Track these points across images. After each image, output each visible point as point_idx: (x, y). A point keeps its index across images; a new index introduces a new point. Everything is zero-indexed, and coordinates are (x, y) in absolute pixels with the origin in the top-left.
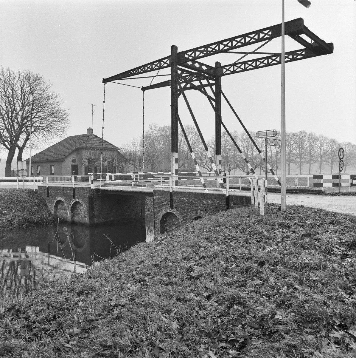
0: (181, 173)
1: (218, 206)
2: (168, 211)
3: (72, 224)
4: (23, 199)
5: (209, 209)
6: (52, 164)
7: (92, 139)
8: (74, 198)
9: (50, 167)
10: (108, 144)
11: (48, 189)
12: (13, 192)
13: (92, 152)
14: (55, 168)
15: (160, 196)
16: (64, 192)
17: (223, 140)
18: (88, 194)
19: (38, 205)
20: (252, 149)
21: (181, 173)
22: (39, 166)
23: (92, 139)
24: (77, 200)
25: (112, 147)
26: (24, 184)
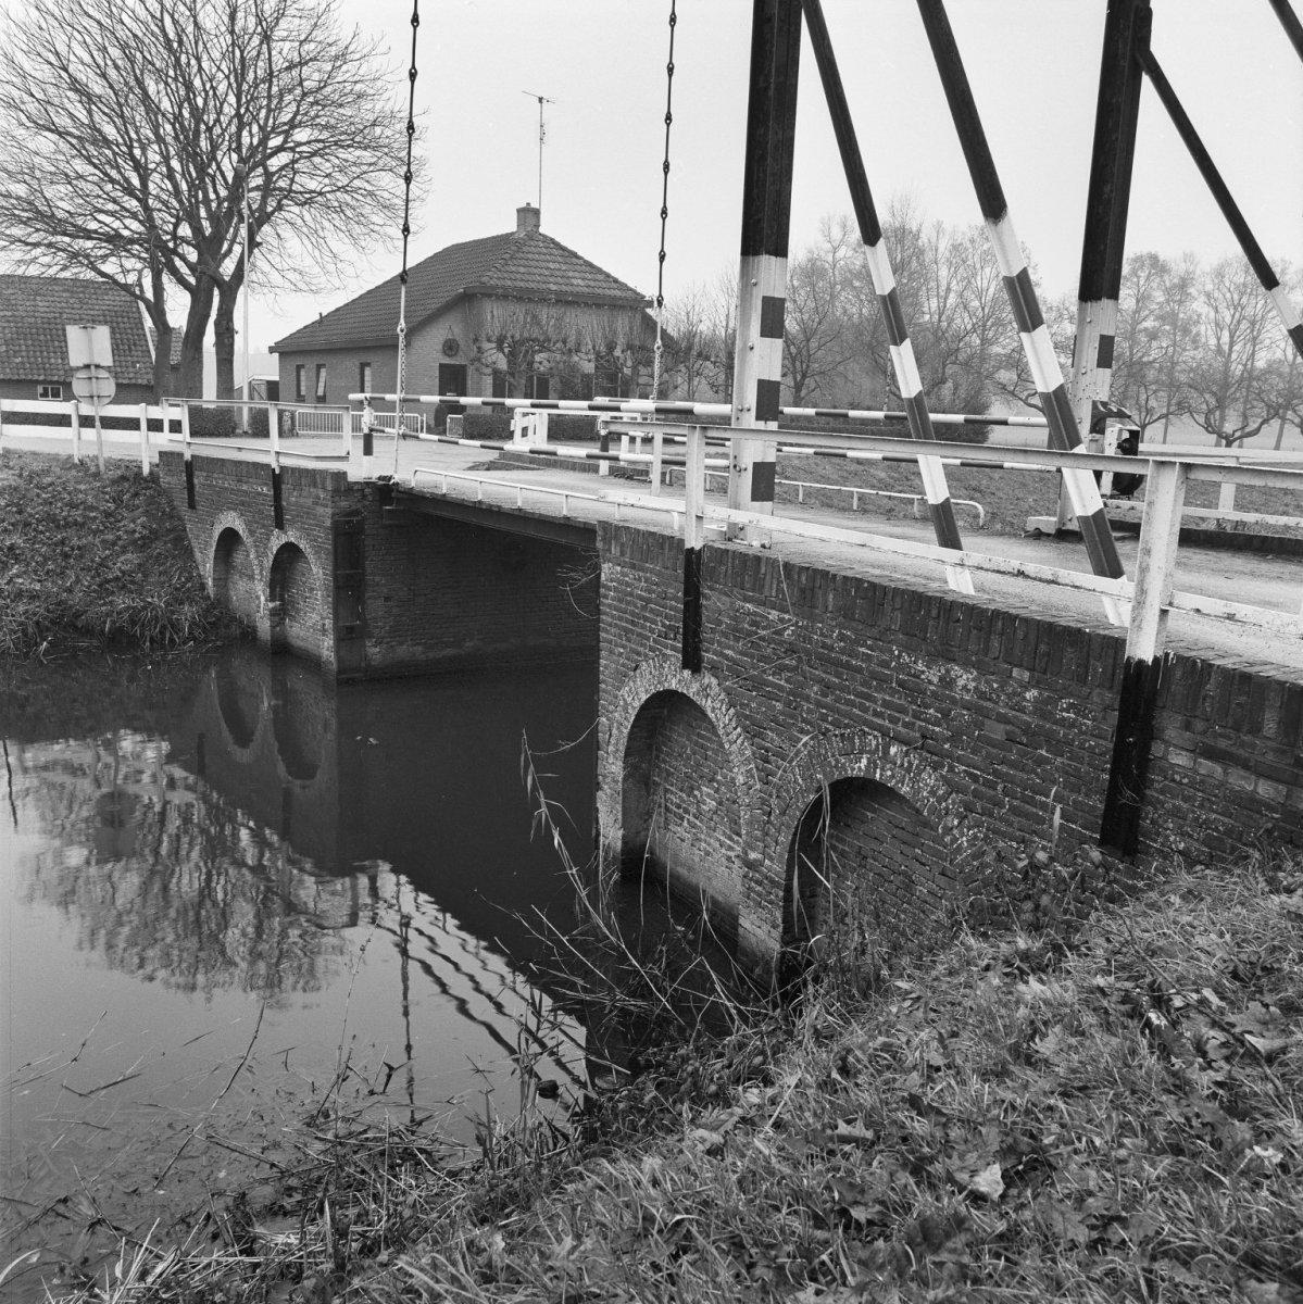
0: (853, 413)
1: (1034, 737)
2: (673, 685)
3: (275, 653)
4: (77, 514)
5: (954, 739)
6: (365, 358)
7: (530, 256)
8: (280, 525)
9: (357, 371)
10: (601, 277)
11: (190, 467)
12: (47, 472)
13: (519, 310)
14: (373, 374)
15: (633, 567)
16: (245, 487)
17: (1127, 292)
18: (329, 511)
19: (143, 544)
20: (1255, 339)
21: (853, 413)
22: (368, 365)
23: (530, 256)
24: (291, 536)
25: (618, 293)
26: (99, 436)
